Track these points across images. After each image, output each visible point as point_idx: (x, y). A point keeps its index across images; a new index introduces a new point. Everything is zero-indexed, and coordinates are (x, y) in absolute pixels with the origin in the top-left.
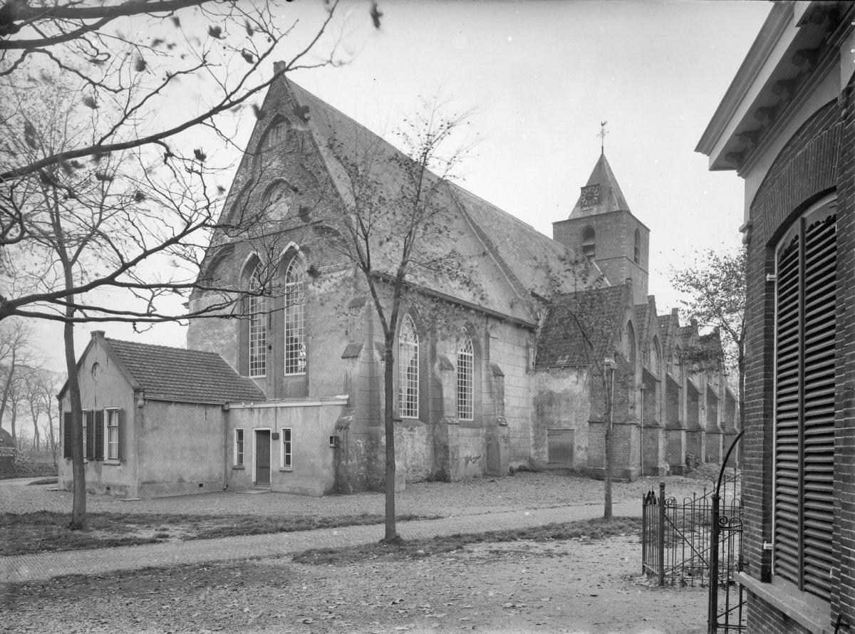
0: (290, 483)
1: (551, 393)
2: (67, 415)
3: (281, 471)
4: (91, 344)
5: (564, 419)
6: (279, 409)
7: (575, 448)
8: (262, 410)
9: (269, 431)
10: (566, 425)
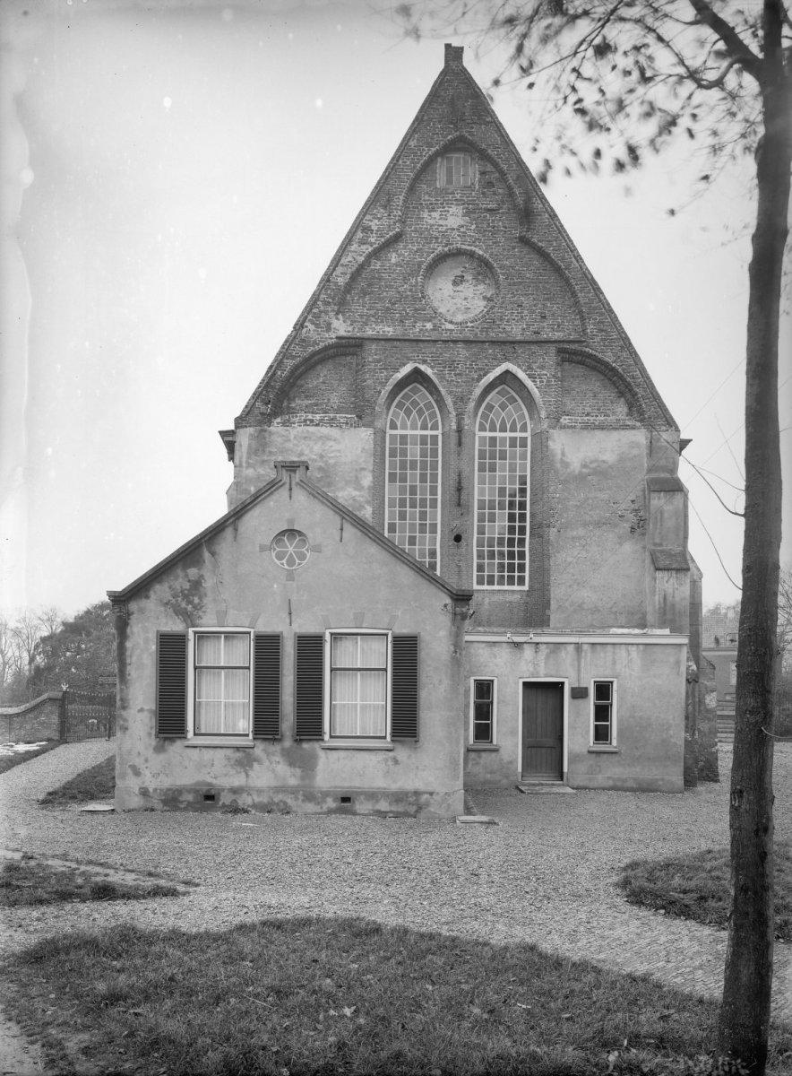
0: (613, 771)
2: (38, 669)
3: (589, 752)
8: (542, 647)
9: (563, 683)
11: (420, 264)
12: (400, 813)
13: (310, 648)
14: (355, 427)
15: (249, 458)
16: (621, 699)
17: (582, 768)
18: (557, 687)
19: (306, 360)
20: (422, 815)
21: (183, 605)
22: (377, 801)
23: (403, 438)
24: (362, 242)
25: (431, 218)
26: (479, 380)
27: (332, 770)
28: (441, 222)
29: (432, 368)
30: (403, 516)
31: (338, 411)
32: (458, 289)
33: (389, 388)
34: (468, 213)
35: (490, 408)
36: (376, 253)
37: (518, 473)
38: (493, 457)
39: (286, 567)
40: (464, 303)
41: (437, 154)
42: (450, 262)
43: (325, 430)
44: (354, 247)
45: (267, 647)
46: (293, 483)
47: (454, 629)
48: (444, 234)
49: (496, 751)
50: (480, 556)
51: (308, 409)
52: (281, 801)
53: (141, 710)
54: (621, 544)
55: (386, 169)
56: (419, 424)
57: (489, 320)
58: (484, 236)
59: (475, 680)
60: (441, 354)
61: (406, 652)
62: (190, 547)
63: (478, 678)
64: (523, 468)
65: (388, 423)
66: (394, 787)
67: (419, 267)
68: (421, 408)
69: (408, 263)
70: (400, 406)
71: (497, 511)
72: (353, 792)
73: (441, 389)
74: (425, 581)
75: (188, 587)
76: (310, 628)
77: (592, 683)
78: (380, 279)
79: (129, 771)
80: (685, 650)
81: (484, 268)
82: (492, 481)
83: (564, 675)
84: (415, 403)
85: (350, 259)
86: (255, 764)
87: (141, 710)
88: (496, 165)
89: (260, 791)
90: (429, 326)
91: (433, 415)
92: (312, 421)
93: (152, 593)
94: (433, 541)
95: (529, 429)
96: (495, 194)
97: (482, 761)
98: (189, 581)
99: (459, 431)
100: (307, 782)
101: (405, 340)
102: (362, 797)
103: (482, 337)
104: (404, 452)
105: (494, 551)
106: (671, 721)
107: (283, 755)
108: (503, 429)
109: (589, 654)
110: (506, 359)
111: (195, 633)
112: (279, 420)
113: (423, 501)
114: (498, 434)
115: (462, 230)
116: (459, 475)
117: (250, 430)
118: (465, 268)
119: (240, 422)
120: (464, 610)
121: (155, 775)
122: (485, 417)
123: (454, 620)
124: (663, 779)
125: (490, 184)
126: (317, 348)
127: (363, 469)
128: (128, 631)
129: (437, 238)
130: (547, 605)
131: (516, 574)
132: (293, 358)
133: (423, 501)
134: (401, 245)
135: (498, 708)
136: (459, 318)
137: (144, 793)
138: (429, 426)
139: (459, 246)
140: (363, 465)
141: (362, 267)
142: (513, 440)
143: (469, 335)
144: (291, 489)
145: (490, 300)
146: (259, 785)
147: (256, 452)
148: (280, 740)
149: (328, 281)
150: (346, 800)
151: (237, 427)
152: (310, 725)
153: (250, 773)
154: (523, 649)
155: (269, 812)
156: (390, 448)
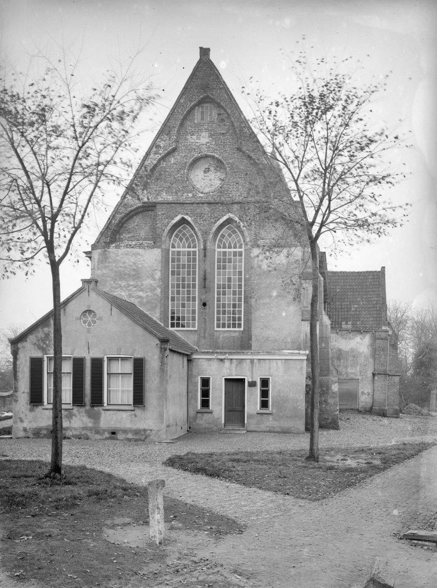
1: (340, 350)
3: (257, 414)
4: (80, 291)
5: (349, 370)
6: (255, 361)
7: (360, 393)
9: (244, 379)
10: (352, 376)
11: (186, 163)
12: (137, 439)
13: (97, 364)
14: (152, 248)
15: (98, 265)
16: (273, 386)
17: (254, 421)
18: (243, 381)
19: (127, 214)
20: (147, 440)
21: (42, 344)
22: (127, 434)
23: (179, 252)
24: (156, 153)
25: (192, 139)
26: (215, 223)
27: (108, 419)
28: (197, 141)
29: (191, 217)
30: (178, 293)
31: (145, 239)
32: (206, 175)
33: (169, 228)
34: (211, 136)
35: (223, 236)
36: (163, 158)
37: (237, 270)
38: (224, 261)
39: (87, 327)
40: (210, 182)
41: (195, 106)
42: (202, 161)
43: (137, 250)
44: (152, 156)
45: (78, 363)
46: (90, 289)
47: (161, 355)
48: (198, 147)
49: (211, 413)
50: (218, 313)
51: (129, 239)
52: (85, 434)
53: (23, 393)
54: (288, 306)
55: (169, 114)
56: (187, 245)
57: (221, 191)
58: (219, 147)
59: (201, 378)
60: (196, 210)
61: (139, 365)
62: (44, 318)
63: (202, 376)
64: (240, 267)
65: (171, 245)
66: (135, 427)
67: (186, 165)
68: (187, 237)
69: (180, 163)
70: (177, 236)
71: (227, 290)
72: (116, 430)
73: (195, 228)
74: (148, 333)
75: (44, 336)
76: (97, 355)
77: (259, 379)
78: (165, 171)
79: (19, 420)
80: (305, 362)
81: (219, 164)
82: (224, 274)
83: (244, 374)
84: (184, 235)
85: (149, 162)
86: (73, 417)
87: (23, 393)
88: (225, 110)
89: (75, 429)
90: (190, 195)
91: (194, 241)
92: (130, 245)
93: (28, 339)
94: (194, 305)
95: (243, 247)
96: (225, 125)
97: (204, 418)
98: (44, 334)
99: (205, 249)
100: (96, 425)
101: (178, 203)
102: (121, 432)
103: (218, 200)
104: (179, 260)
105: (225, 310)
106: (298, 398)
107: (85, 413)
108: (230, 247)
109: (257, 364)
110: (229, 212)
111: (47, 357)
112: (114, 245)
113: (189, 285)
114: (227, 250)
115: (208, 144)
116: (205, 272)
117: (99, 251)
118: (210, 163)
119: (94, 247)
120: (165, 346)
121: (30, 422)
122: (220, 241)
123: (161, 351)
124: (294, 427)
125: (223, 120)
126: (132, 208)
127: (155, 270)
128: (18, 356)
129: (195, 149)
130: (250, 338)
131: (237, 322)
132: (121, 213)
133: (189, 285)
134: (176, 153)
135: (212, 391)
136: (207, 190)
137: (25, 430)
138: (192, 246)
139: (206, 153)
140: (156, 268)
141: (155, 166)
142: (235, 253)
143: (210, 199)
144: (89, 292)
145: (223, 180)
146: (75, 426)
147: (102, 262)
148: (84, 406)
149: (138, 174)
150: (113, 433)
151: (92, 250)
152: (97, 399)
153: (71, 421)
154: (225, 362)
155: (79, 439)
156: (172, 258)
